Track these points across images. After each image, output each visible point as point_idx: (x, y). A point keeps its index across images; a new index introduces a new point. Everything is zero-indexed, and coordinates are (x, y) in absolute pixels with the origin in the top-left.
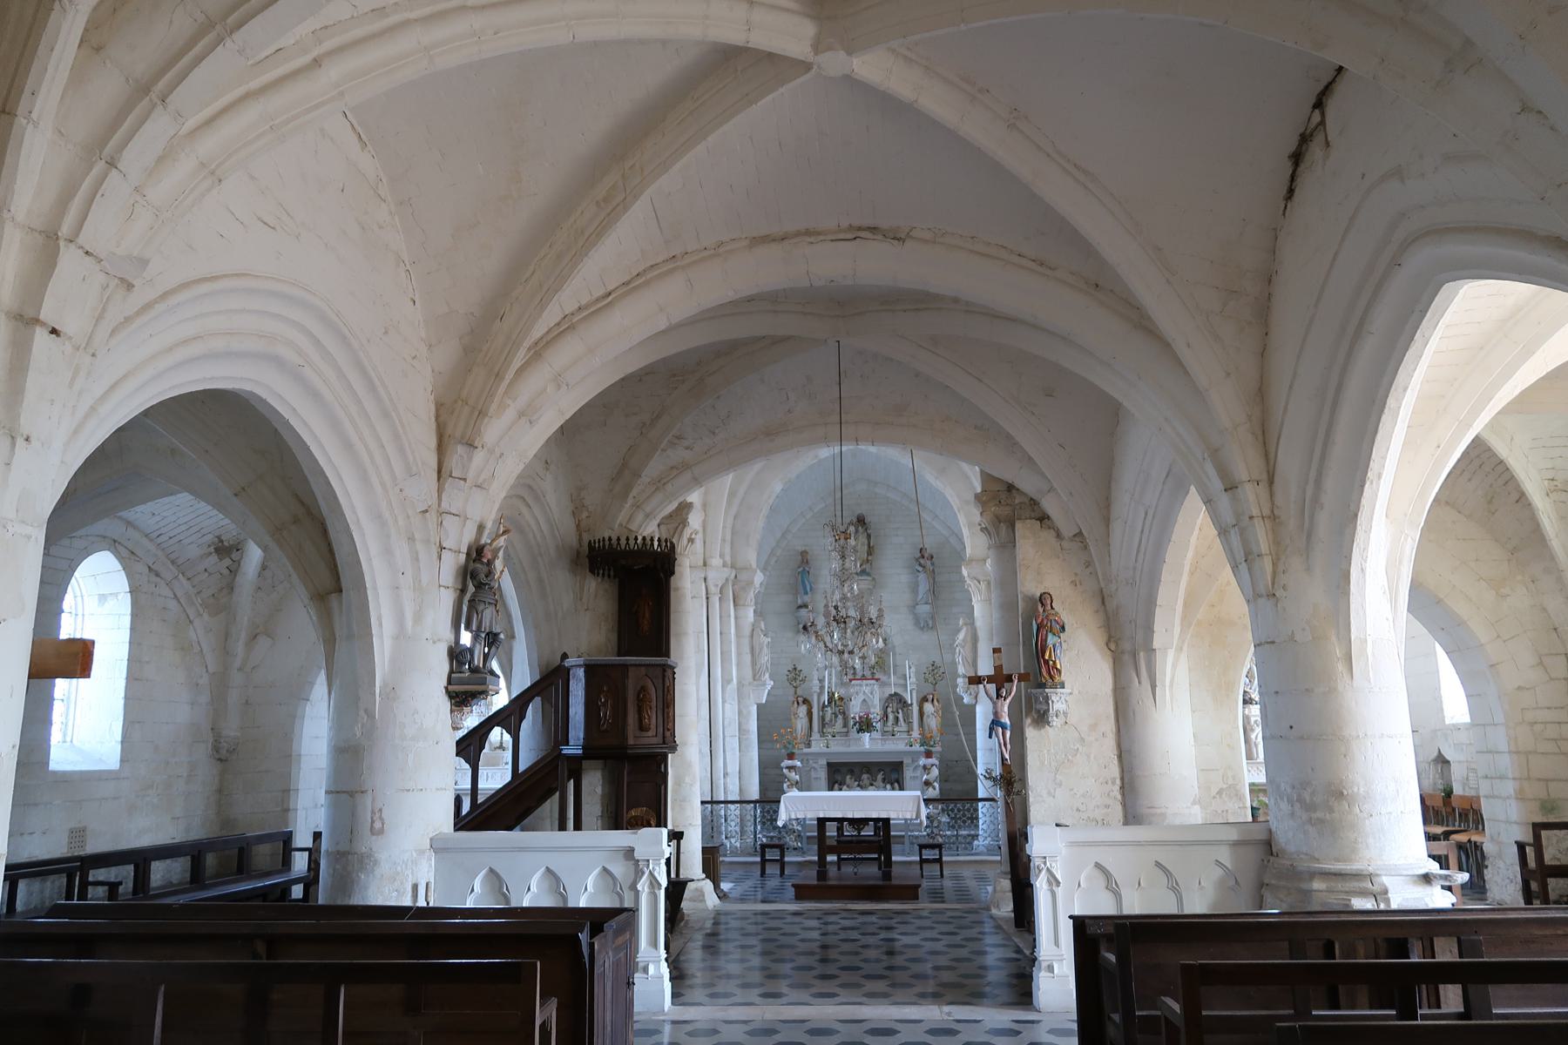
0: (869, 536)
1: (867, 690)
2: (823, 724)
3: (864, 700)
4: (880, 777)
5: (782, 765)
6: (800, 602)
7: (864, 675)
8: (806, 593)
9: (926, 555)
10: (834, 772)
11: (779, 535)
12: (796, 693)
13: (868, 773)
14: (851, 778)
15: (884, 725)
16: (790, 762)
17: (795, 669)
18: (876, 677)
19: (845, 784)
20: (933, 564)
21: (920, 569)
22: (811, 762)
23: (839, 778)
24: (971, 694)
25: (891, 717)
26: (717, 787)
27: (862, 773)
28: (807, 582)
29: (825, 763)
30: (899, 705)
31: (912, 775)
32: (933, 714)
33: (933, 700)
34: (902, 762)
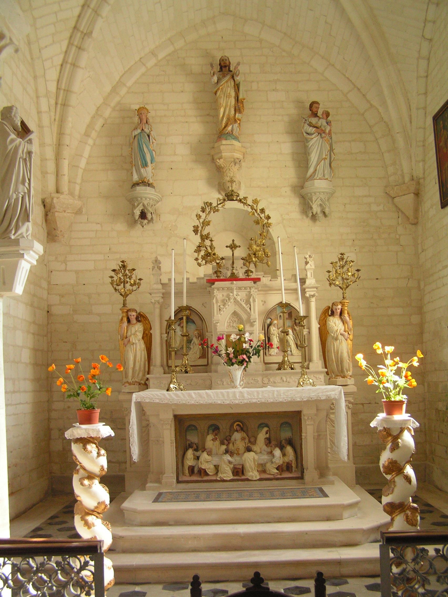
1: (241, 296)
3: (235, 313)
4: (262, 436)
5: (68, 434)
6: (136, 178)
7: (233, 274)
9: (320, 114)
11: (108, 88)
13: (242, 429)
17: (124, 267)
18: (253, 276)
19: (204, 450)
21: (312, 130)
23: (193, 438)
27: (232, 430)
29: (171, 417)
32: (341, 334)
33: (341, 314)
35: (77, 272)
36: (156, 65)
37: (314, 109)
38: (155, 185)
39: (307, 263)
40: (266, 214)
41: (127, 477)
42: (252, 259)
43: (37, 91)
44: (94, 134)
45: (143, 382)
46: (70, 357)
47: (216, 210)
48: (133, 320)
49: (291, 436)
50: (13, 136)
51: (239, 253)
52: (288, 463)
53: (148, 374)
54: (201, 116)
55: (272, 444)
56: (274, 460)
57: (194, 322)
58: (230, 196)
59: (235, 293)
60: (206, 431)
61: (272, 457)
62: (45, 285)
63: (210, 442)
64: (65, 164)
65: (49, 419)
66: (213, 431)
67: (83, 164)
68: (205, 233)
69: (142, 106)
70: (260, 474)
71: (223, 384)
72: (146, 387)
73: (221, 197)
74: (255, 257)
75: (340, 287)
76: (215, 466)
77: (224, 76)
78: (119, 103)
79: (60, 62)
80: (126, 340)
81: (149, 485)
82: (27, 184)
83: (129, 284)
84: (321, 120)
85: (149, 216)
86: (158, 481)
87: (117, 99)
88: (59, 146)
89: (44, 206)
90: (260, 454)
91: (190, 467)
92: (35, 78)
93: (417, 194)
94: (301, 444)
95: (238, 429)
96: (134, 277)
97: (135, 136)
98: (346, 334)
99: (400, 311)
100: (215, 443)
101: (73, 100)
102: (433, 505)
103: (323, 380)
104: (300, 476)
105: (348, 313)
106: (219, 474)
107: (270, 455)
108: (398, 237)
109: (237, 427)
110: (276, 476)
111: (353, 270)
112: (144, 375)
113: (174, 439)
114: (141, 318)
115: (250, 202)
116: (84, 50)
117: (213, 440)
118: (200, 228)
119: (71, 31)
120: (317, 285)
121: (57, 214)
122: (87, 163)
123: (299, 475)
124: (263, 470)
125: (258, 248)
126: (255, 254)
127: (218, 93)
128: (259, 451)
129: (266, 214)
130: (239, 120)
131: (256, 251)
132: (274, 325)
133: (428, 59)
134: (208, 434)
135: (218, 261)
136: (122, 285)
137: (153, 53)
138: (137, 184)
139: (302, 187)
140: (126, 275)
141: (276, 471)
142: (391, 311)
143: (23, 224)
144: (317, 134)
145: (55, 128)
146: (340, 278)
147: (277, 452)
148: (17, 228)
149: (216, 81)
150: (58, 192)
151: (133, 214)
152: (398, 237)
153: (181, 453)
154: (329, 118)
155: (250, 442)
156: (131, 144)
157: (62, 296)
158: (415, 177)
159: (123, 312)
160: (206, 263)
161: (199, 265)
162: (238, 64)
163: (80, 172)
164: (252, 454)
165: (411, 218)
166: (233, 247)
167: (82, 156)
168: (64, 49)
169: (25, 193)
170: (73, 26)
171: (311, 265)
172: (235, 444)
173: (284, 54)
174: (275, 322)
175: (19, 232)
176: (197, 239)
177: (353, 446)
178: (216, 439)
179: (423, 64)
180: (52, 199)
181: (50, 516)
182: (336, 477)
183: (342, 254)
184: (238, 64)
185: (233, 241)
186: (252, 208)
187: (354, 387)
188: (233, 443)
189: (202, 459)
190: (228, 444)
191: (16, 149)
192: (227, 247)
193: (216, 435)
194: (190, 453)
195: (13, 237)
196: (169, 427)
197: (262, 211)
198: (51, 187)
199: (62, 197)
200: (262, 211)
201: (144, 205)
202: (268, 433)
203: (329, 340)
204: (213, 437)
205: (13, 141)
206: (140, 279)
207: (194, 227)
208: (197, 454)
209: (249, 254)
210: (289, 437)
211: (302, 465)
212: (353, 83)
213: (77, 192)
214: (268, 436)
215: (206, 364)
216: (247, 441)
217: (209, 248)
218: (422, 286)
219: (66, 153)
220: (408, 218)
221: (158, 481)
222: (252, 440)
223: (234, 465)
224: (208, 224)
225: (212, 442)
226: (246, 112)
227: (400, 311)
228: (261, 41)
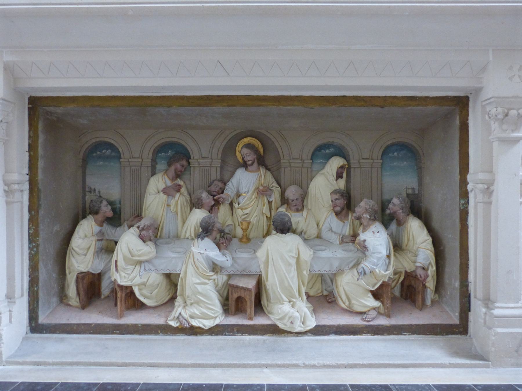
10: (85, 162)
49: (416, 187)
52: (410, 276)
55: (359, 210)
56: (366, 265)
60: (148, 162)
61: (360, 254)
70: (315, 311)
76: (168, 276)
90: (317, 241)
91: (81, 277)
95: (247, 158)
100: (173, 202)
102: (312, 182)
104: (456, 321)
106: (176, 304)
107: (351, 246)
109: (245, 151)
110: (373, 319)
117: (165, 191)
124: (325, 293)
128: (312, 231)
134: (154, 174)
141: (373, 303)
155: (284, 201)
172: (236, 205)
178: (178, 189)
188: (231, 204)
190: (213, 206)
193: (178, 175)
202: (345, 175)
204: (169, 183)
210: (410, 191)
214: (342, 184)
216: (276, 197)
222: (292, 193)
223: (230, 276)
225: (165, 197)
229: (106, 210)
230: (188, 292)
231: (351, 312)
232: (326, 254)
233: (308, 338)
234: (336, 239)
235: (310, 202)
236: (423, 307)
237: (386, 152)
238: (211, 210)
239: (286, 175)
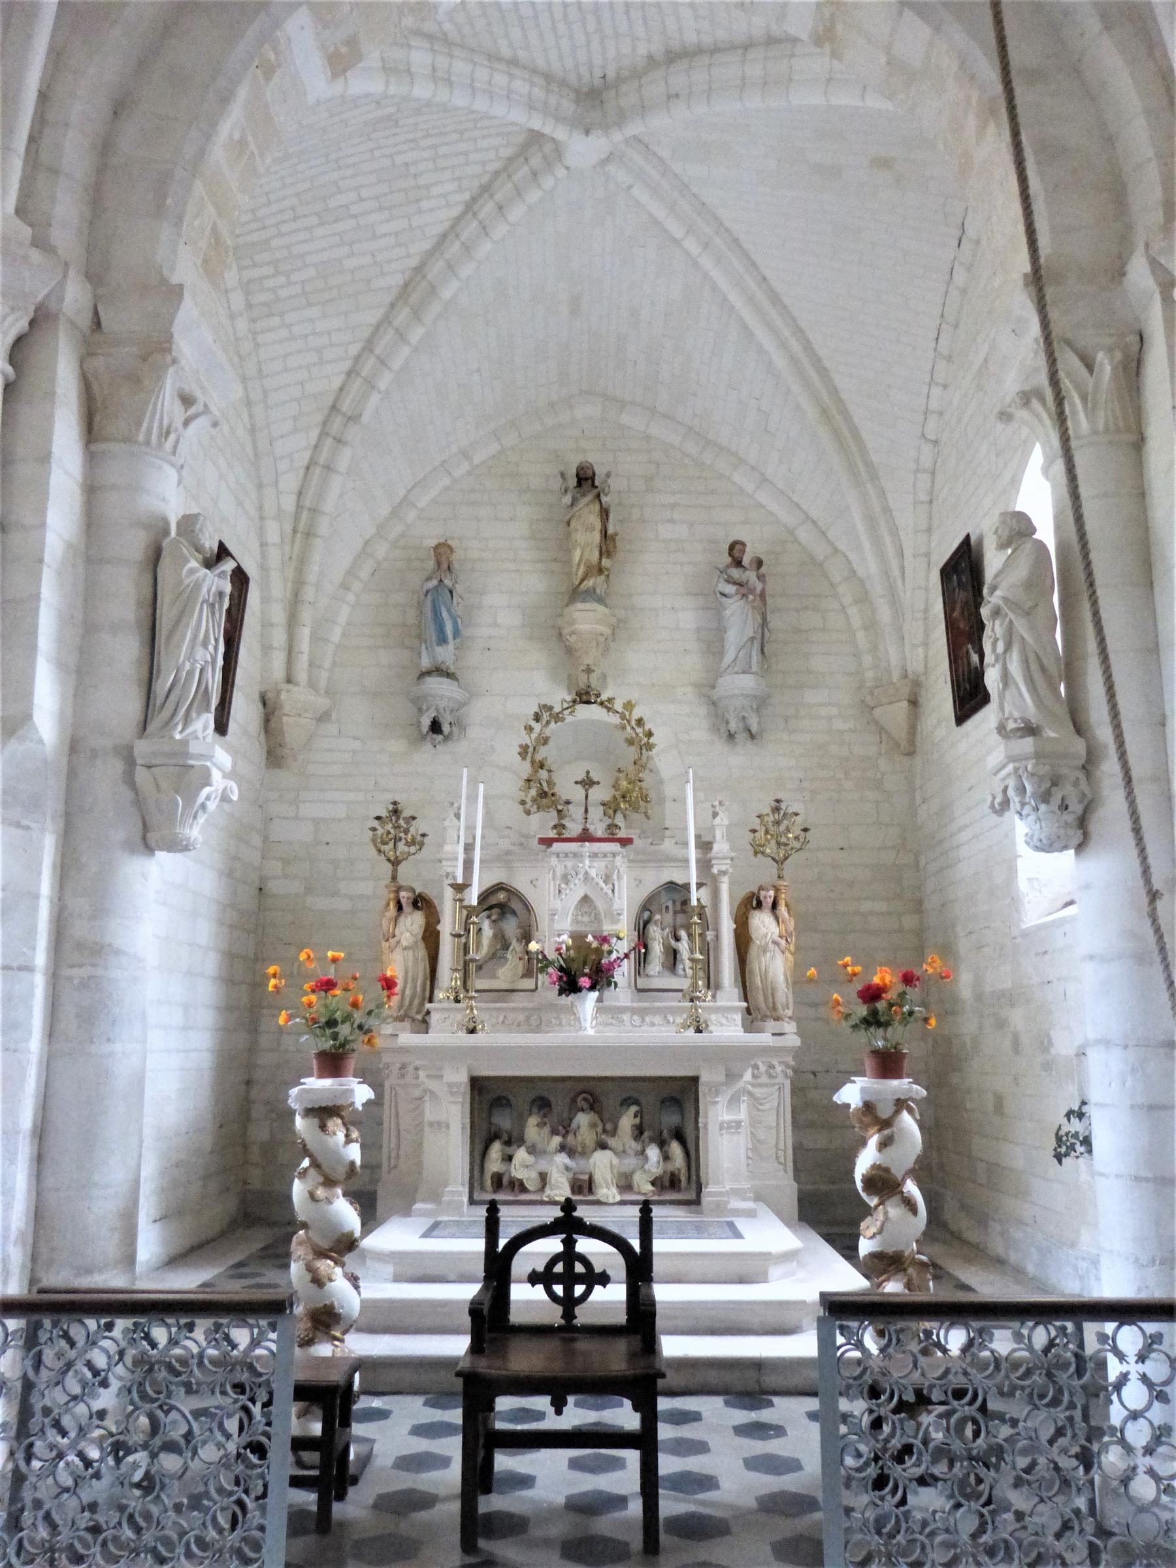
0: (605, 513)
1: (597, 870)
2: (466, 970)
3: (586, 899)
4: (627, 1121)
6: (426, 663)
7: (585, 830)
8: (442, 640)
9: (746, 560)
11: (385, 510)
12: (394, 878)
13: (592, 1108)
14: (541, 1125)
15: (638, 973)
16: (327, 1083)
17: (396, 812)
18: (622, 834)
19: (521, 1141)
20: (761, 578)
21: (730, 589)
22: (421, 1073)
23: (503, 1121)
24: (1064, 807)
25: (657, 949)
26: (751, 972)
27: (574, 1108)
28: (445, 614)
30: (680, 919)
31: (727, 1117)
32: (775, 943)
33: (774, 906)
34: (695, 1080)
35: (317, 822)
36: (469, 473)
37: (736, 553)
38: (459, 676)
39: (715, 815)
40: (647, 728)
41: (381, 1193)
42: (619, 804)
43: (261, 508)
44: (357, 586)
45: (419, 1017)
46: (295, 971)
47: (558, 718)
48: (407, 908)
50: (194, 564)
51: (600, 794)
52: (673, 1174)
53: (431, 1001)
54: (542, 561)
56: (647, 1167)
57: (514, 913)
58: (584, 697)
59: (587, 862)
62: (257, 840)
63: (533, 1129)
64: (305, 633)
65: (248, 1083)
66: (540, 1108)
67: (336, 635)
68: (538, 757)
69: (442, 541)
71: (560, 1024)
72: (423, 1026)
73: (569, 698)
74: (625, 802)
75: (774, 859)
77: (584, 495)
78: (403, 535)
79: (306, 462)
80: (393, 941)
81: (418, 1206)
82: (211, 648)
83: (403, 841)
84: (747, 573)
85: (446, 729)
86: (435, 1197)
87: (399, 528)
88: (295, 601)
89: (264, 704)
92: (260, 486)
93: (914, 703)
94: (697, 1138)
96: (412, 830)
97: (427, 592)
98: (783, 942)
99: (882, 906)
101: (323, 526)
103: (739, 1022)
105: (787, 905)
108: (879, 776)
111: (797, 831)
112: (422, 1004)
113: (468, 1120)
114: (421, 902)
115: (618, 706)
116: (345, 443)
117: (538, 1125)
118: (531, 750)
119: (326, 412)
120: (733, 854)
121: (285, 719)
122: (344, 635)
123: (691, 1196)
125: (630, 787)
126: (624, 797)
127: (573, 524)
128: (620, 1148)
129: (647, 728)
130: (607, 569)
131: (628, 791)
132: (656, 923)
133: (933, 473)
134: (530, 1114)
135: (560, 807)
136: (391, 844)
137: (465, 454)
138: (429, 673)
139: (713, 687)
140: (399, 827)
141: (650, 1188)
142: (866, 906)
143: (199, 714)
144: (740, 596)
145: (290, 573)
146: (773, 842)
147: (653, 1153)
148: (187, 721)
149: (569, 503)
150: (289, 681)
151: (418, 724)
152: (879, 776)
153: (479, 1148)
154: (763, 570)
155: (605, 1131)
156: (420, 605)
157: (286, 862)
158: (909, 672)
159: (390, 892)
160: (538, 808)
161: (528, 813)
162: (608, 475)
163: (330, 649)
164: (608, 1153)
165: (904, 744)
166: (588, 783)
167: (334, 622)
168: (313, 442)
169: (206, 662)
170: (330, 404)
171: (723, 820)
173: (686, 461)
174: (658, 917)
175: (188, 731)
176: (526, 768)
177: (794, 1149)
178: (545, 1124)
179: (924, 481)
180: (278, 692)
181: (231, 1263)
182: (761, 1204)
183: (778, 801)
184: (608, 475)
185: (588, 772)
186: (623, 717)
187: (796, 1037)
189: (516, 1160)
191: (198, 586)
192: (576, 783)
193: (545, 1116)
194: (496, 1149)
195: (178, 737)
196: (460, 1099)
197: (640, 722)
198: (278, 673)
199: (295, 689)
200: (640, 722)
201: (437, 710)
203: (753, 951)
205: (192, 571)
206: (423, 835)
207: (521, 746)
208: (509, 1150)
209: (614, 796)
211: (698, 1176)
212: (805, 512)
213: (323, 684)
214: (638, 1121)
215: (533, 987)
216: (600, 1129)
217: (545, 784)
218: (922, 863)
219: (306, 615)
220: (898, 745)
221: (435, 1197)
224: (545, 741)
226: (620, 556)
227: (882, 906)
228: (648, 438)
229: (505, 1137)
230: (553, 1182)
231: (640, 1193)
232: (626, 1161)
233: (616, 1207)
234: (632, 1153)
235: (619, 1132)
236: (679, 1190)
237: (663, 1102)
238: (564, 1136)
239: (606, 1115)
